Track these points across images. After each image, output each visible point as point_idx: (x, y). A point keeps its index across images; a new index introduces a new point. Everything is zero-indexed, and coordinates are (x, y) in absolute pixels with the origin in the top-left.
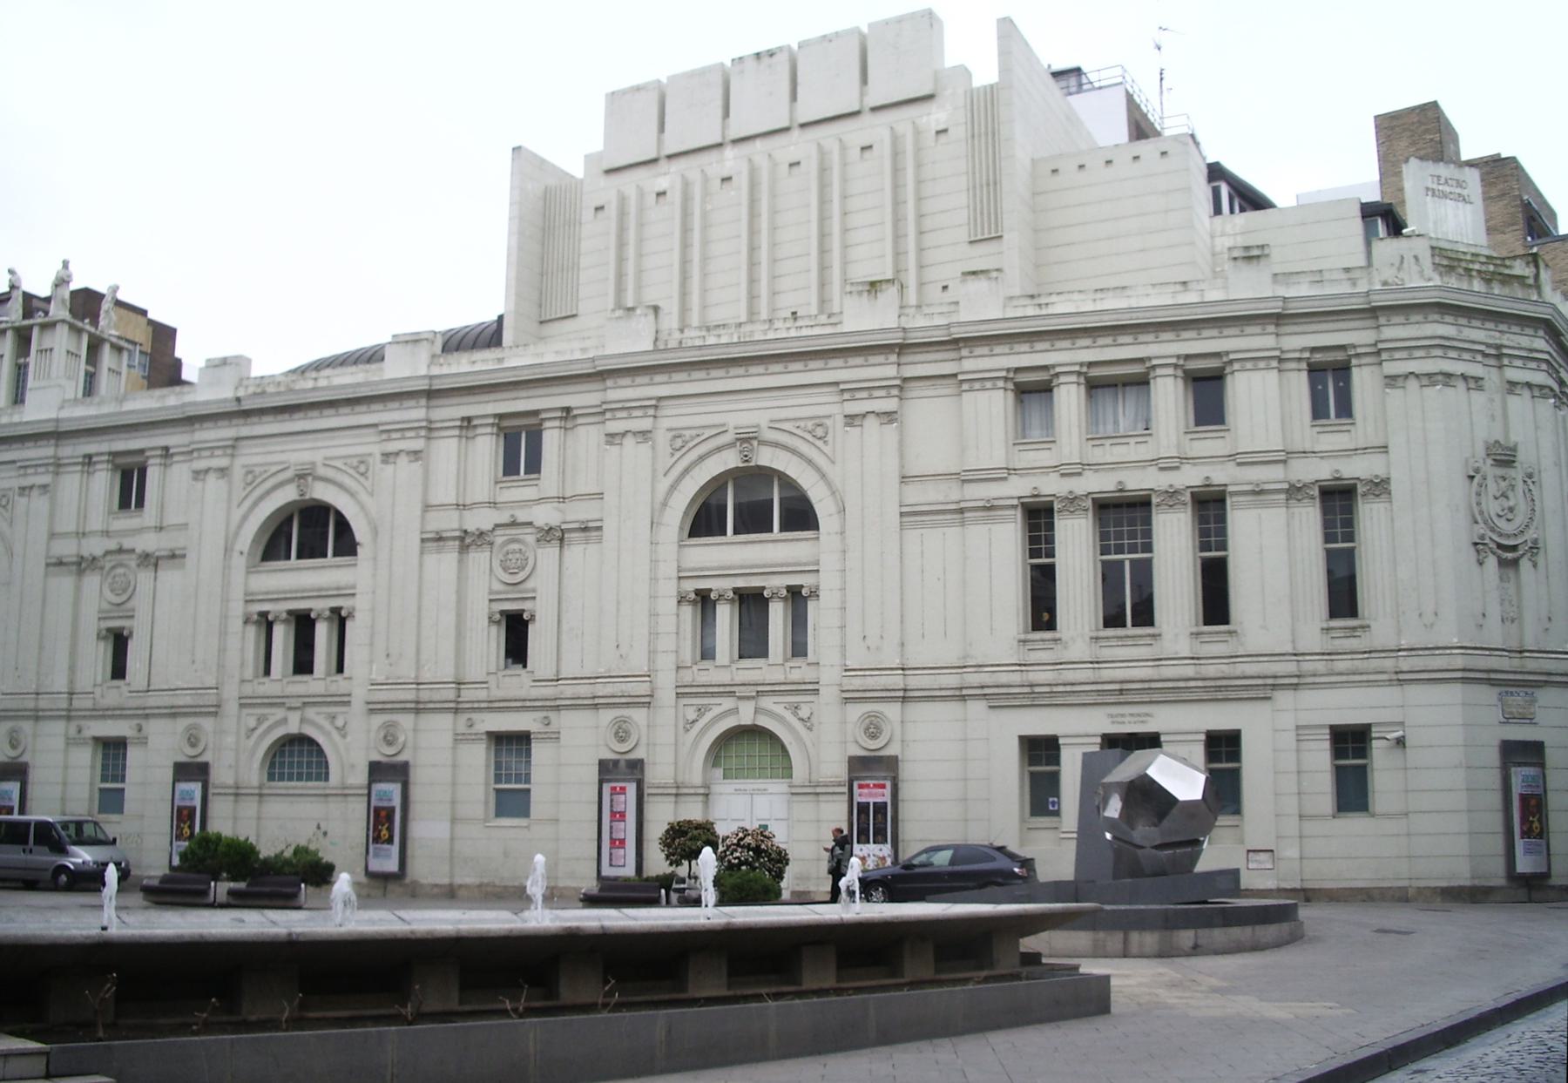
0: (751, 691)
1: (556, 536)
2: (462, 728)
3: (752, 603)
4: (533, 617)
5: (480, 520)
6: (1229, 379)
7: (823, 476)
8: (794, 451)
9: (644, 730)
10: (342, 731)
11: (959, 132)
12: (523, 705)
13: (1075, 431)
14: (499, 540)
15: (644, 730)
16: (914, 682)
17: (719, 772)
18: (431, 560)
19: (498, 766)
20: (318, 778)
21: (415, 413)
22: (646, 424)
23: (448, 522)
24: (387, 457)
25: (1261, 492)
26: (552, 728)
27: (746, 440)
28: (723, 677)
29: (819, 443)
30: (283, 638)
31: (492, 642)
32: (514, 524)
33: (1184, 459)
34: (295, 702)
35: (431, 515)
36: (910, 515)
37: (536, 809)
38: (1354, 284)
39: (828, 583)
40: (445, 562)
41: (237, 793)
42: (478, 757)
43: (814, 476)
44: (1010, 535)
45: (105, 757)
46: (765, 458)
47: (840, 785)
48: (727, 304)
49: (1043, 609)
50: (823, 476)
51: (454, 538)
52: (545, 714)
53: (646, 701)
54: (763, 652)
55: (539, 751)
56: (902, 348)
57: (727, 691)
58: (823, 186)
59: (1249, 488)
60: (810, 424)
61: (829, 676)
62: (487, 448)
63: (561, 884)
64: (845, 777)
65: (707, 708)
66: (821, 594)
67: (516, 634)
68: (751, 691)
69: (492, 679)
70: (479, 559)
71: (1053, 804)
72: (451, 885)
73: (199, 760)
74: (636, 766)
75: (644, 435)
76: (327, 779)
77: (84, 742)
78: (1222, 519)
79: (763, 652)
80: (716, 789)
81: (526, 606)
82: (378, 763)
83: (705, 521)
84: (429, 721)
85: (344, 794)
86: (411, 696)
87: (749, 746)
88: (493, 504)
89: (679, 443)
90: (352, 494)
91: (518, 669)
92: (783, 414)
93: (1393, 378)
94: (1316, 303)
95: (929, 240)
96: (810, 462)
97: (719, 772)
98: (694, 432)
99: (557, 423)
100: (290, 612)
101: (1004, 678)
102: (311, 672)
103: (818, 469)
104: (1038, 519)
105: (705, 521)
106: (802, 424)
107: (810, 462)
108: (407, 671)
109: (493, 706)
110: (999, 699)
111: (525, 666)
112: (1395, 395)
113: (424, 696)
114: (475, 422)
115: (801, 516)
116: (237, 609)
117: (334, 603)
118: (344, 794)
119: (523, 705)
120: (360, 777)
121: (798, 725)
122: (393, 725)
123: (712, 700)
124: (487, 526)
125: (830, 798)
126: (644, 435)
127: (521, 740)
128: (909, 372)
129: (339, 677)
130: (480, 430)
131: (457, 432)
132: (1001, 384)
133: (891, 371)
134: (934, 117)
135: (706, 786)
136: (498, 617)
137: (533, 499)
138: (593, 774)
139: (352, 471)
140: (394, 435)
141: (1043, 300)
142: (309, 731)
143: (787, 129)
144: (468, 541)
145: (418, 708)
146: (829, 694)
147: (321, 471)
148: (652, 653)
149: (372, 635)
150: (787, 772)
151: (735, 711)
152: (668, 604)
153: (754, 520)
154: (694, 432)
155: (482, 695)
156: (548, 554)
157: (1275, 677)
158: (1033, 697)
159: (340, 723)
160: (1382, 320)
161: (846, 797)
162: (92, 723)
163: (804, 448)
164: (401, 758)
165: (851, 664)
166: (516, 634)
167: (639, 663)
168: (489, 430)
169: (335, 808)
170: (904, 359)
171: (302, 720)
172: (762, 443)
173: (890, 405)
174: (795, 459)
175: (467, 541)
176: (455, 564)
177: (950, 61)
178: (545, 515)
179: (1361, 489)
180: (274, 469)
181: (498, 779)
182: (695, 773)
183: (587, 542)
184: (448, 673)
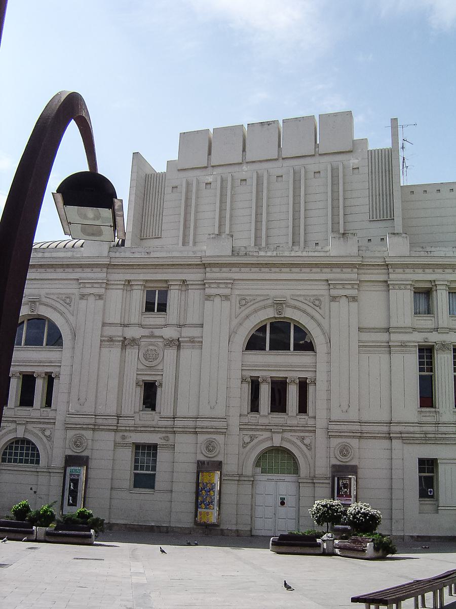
0: (280, 429)
1: (177, 344)
2: (119, 440)
3: (279, 388)
4: (161, 385)
5: (131, 333)
6: (169, 292)
7: (319, 325)
8: (304, 312)
9: (222, 446)
10: (49, 438)
11: (365, 170)
12: (154, 430)
13: (137, 313)
14: (143, 344)
15: (222, 446)
16: (365, 428)
17: (259, 470)
18: (105, 351)
19: (136, 461)
20: (32, 462)
21: (100, 275)
22: (227, 291)
23: (117, 332)
24: (83, 297)
25: (406, 346)
26: (171, 442)
27: (279, 304)
28: (263, 421)
29: (317, 308)
30: (265, 392)
31: (136, 396)
32: (152, 336)
33: (414, 329)
34: (146, 427)
35: (106, 328)
36: (363, 347)
37: (158, 485)
38: (266, 253)
39: (64, 372)
40: (113, 354)
41: (240, 478)
42: (127, 455)
43: (315, 325)
44: (412, 360)
45: (137, 454)
46: (289, 313)
47: (326, 478)
48: (245, 238)
49: (427, 399)
50: (319, 325)
51: (119, 341)
52: (166, 435)
53: (224, 432)
54: (30, 404)
55: (162, 456)
56: (360, 266)
57: (268, 428)
58: (296, 189)
59: (188, 339)
60: (64, 297)
61: (60, 417)
62: (138, 298)
63: (173, 525)
64: (329, 475)
65: (255, 437)
66: (61, 376)
67: (150, 394)
68: (280, 429)
69: (137, 416)
70: (132, 353)
71: (431, 492)
72: (404, 536)
73: (215, 459)
74: (218, 465)
75: (227, 297)
76: (38, 462)
77: (125, 445)
78: (431, 357)
79: (30, 404)
80: (257, 478)
81: (157, 378)
82: (70, 456)
83: (254, 343)
84: (100, 435)
85: (49, 471)
86: (92, 421)
87: (278, 459)
88: (141, 326)
89: (317, 303)
90: (62, 314)
91: (149, 412)
92: (298, 293)
93: (209, 296)
94: (165, 260)
95: (350, 218)
96: (312, 317)
97: (259, 470)
98: (251, 298)
99: (177, 287)
100: (21, 373)
101: (411, 429)
102: (32, 406)
103: (315, 320)
104: (426, 353)
105: (254, 343)
106: (60, 296)
107: (312, 317)
108: (89, 408)
109: (136, 430)
110: (407, 439)
111: (154, 409)
112: (208, 304)
113: (100, 421)
114: (133, 283)
115: (56, 339)
116: (237, 375)
117: (48, 370)
118: (49, 471)
119: (154, 430)
120: (59, 462)
121: (45, 439)
122: (81, 437)
123: (258, 433)
124: (137, 336)
125: (8, 472)
126: (227, 297)
127: (152, 449)
128: (363, 278)
129: (48, 409)
130: (135, 287)
131: (122, 287)
132: (409, 287)
133: (355, 276)
134: (353, 161)
135: (253, 476)
136: (141, 383)
137: (164, 326)
138: (193, 468)
139: (61, 302)
140: (87, 285)
141: (428, 249)
142: (29, 437)
143: (314, 155)
144: (126, 342)
145: (95, 428)
146: (320, 434)
147: (44, 300)
148: (227, 407)
149: (70, 388)
150: (296, 470)
151: (16, 430)
152: (236, 382)
153: (280, 345)
154: (251, 298)
155: (131, 423)
156: (171, 353)
157: (445, 434)
158: (426, 439)
159: (47, 433)
160: (208, 269)
161: (62, 475)
162: (132, 434)
163: (309, 310)
164: (353, 463)
165: (333, 419)
166: (150, 394)
167: (220, 412)
168: (140, 287)
169: (43, 479)
170: (110, 270)
171: (26, 430)
172: (41, 304)
173: (353, 292)
174: (49, 309)
175: (126, 343)
176: (119, 354)
177: (357, 136)
178: (170, 333)
179: (436, 347)
180: (259, 299)
181: (136, 468)
182: (249, 469)
183: (193, 348)
184: (112, 409)
